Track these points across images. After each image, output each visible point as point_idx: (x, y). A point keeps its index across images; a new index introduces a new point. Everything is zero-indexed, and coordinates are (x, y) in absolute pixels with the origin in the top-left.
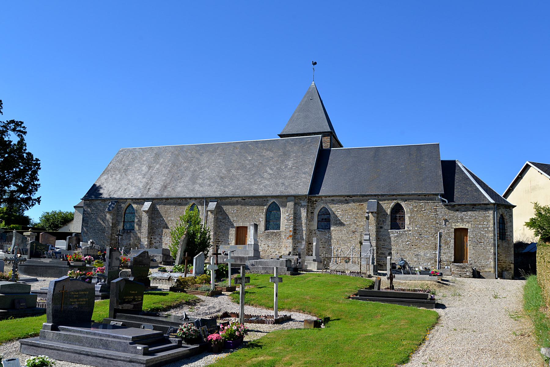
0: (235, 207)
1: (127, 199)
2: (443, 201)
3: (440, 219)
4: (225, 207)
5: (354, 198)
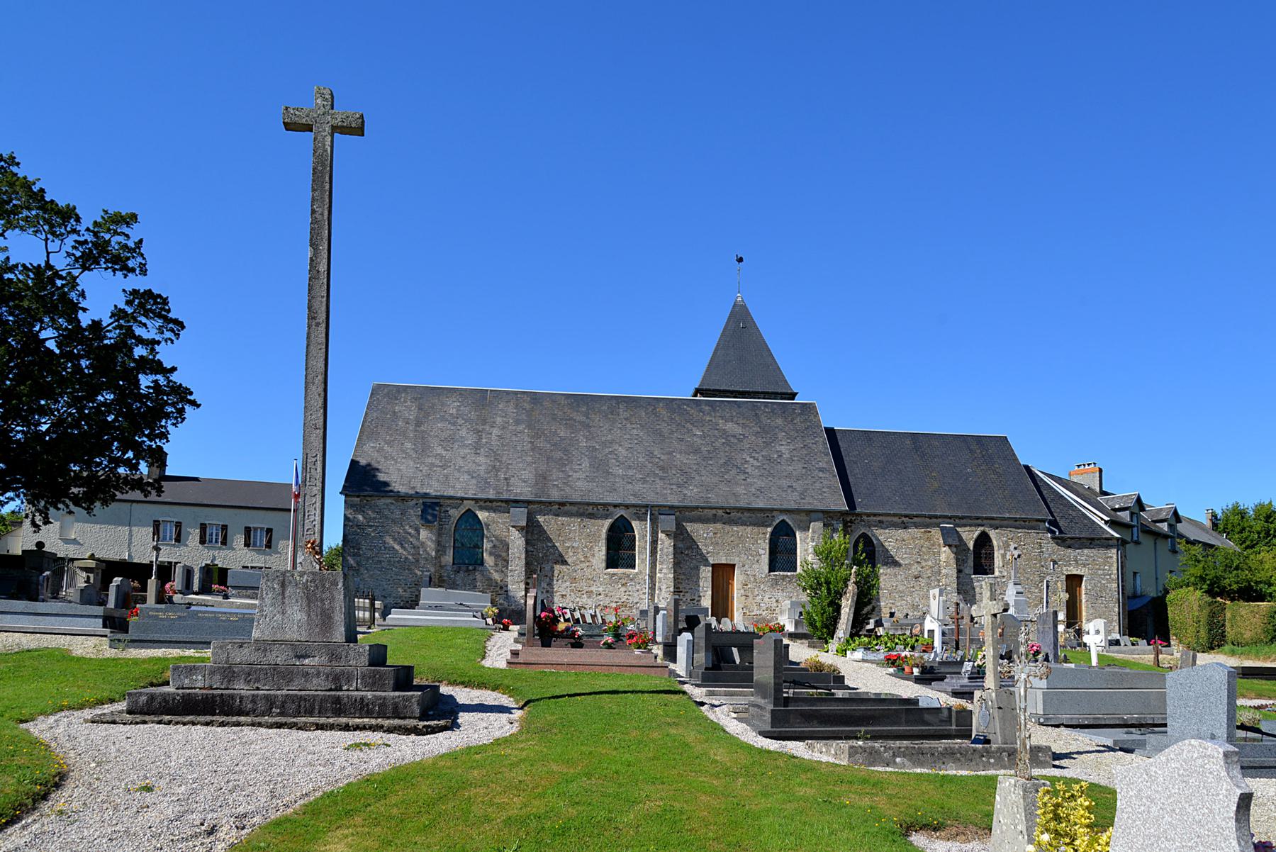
0: (711, 527)
1: (462, 499)
2: (1053, 532)
3: (1046, 560)
4: (689, 527)
5: (915, 520)
